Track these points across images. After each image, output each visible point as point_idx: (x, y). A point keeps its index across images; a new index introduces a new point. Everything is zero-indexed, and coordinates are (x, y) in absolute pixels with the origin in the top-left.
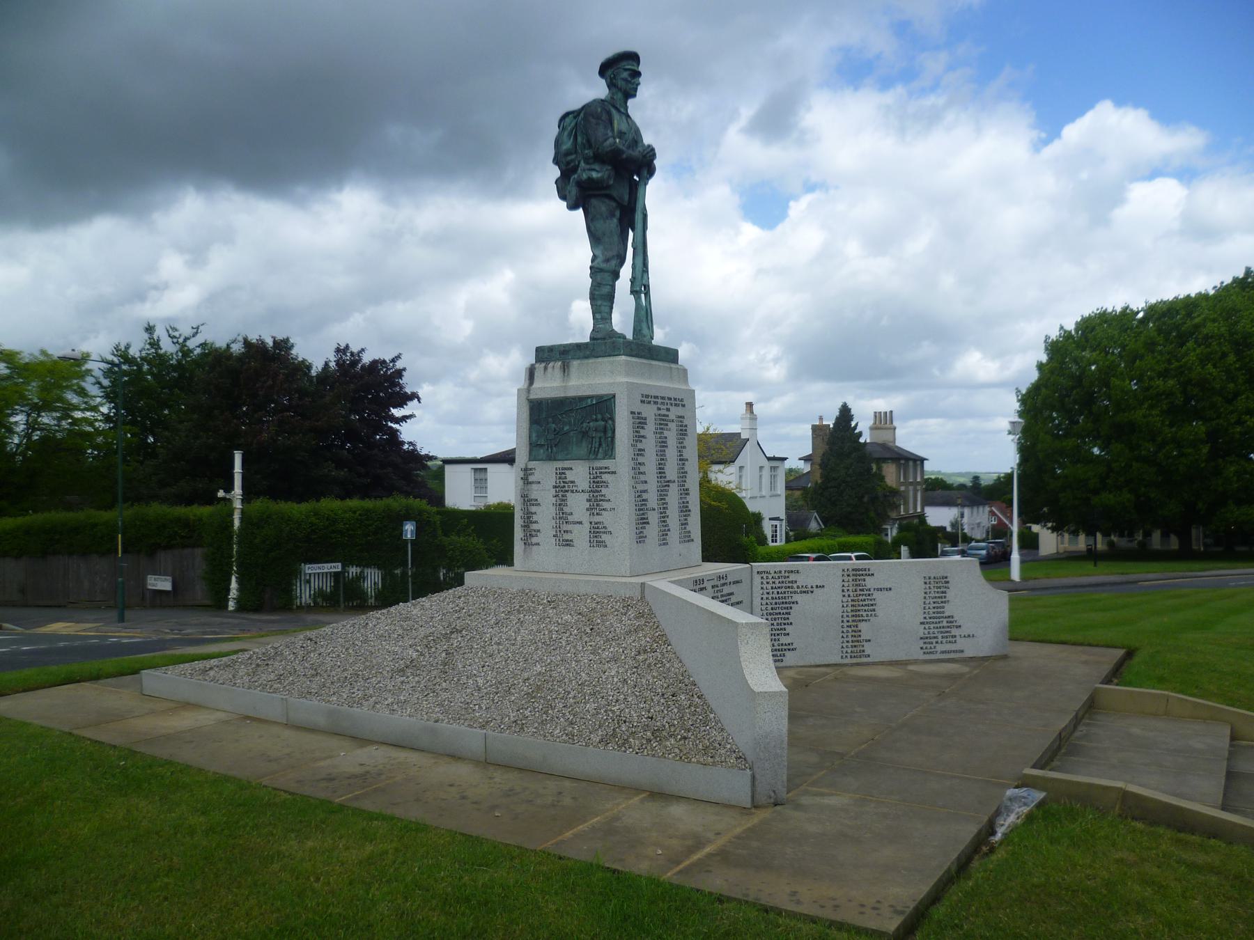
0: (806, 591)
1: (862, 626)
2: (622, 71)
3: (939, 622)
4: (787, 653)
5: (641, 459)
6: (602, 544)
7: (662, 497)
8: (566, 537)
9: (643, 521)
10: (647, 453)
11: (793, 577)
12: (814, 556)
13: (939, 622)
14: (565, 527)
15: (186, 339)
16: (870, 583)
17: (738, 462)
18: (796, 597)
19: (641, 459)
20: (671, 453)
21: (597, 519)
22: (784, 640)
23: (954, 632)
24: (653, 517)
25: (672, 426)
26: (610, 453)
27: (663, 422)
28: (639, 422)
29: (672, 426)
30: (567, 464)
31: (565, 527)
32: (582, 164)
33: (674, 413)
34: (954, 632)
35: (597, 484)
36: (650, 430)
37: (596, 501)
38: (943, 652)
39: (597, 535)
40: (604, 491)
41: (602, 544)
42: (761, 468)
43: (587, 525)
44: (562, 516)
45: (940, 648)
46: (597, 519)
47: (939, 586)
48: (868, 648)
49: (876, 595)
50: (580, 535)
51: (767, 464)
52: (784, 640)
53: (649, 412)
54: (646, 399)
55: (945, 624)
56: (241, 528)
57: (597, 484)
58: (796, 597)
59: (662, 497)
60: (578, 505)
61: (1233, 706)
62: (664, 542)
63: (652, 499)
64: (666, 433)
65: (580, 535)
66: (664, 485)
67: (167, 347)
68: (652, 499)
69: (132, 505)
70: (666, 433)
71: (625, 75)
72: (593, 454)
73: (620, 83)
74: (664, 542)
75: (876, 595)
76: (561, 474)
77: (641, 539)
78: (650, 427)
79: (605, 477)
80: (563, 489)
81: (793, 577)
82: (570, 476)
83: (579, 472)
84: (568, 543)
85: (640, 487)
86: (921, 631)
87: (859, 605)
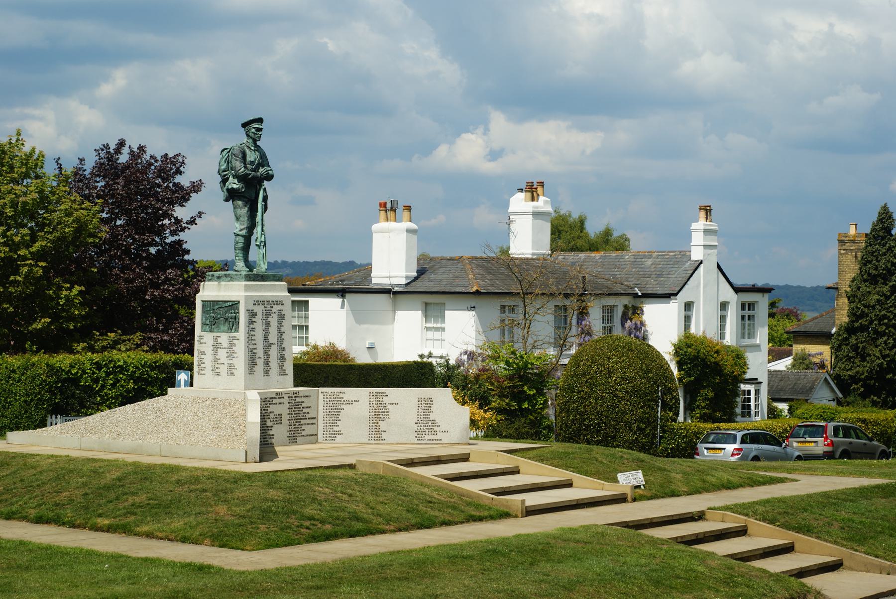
0: (348, 403)
1: (380, 423)
2: (253, 126)
3: (426, 424)
5: (252, 333)
6: (232, 374)
7: (266, 352)
8: (218, 370)
9: (253, 363)
10: (257, 330)
11: (341, 395)
13: (426, 424)
14: (217, 366)
16: (386, 400)
17: (684, 296)
18: (343, 406)
19: (252, 333)
20: (273, 330)
21: (231, 362)
22: (336, 429)
23: (436, 429)
24: (260, 362)
25: (274, 315)
26: (237, 330)
27: (268, 314)
28: (252, 314)
29: (274, 315)
30: (218, 334)
31: (217, 366)
32: (231, 178)
33: (275, 308)
34: (436, 429)
35: (232, 344)
36: (259, 319)
37: (231, 354)
39: (231, 368)
40: (234, 348)
41: (232, 374)
42: (724, 306)
43: (226, 365)
44: (216, 360)
45: (427, 437)
46: (231, 362)
47: (428, 403)
48: (384, 435)
49: (389, 407)
50: (223, 369)
51: (728, 294)
52: (336, 429)
53: (259, 310)
54: (257, 303)
57: (232, 344)
58: (343, 406)
59: (266, 352)
60: (222, 354)
62: (267, 372)
63: (260, 352)
64: (269, 319)
65: (223, 369)
66: (268, 345)
68: (260, 352)
70: (269, 319)
71: (253, 130)
72: (230, 330)
73: (251, 134)
74: (267, 372)
75: (389, 407)
76: (216, 338)
77: (251, 372)
78: (259, 319)
79: (235, 341)
80: (216, 346)
81: (341, 395)
82: (219, 340)
83: (224, 338)
84: (218, 374)
85: (252, 347)
86: (416, 427)
87: (379, 414)
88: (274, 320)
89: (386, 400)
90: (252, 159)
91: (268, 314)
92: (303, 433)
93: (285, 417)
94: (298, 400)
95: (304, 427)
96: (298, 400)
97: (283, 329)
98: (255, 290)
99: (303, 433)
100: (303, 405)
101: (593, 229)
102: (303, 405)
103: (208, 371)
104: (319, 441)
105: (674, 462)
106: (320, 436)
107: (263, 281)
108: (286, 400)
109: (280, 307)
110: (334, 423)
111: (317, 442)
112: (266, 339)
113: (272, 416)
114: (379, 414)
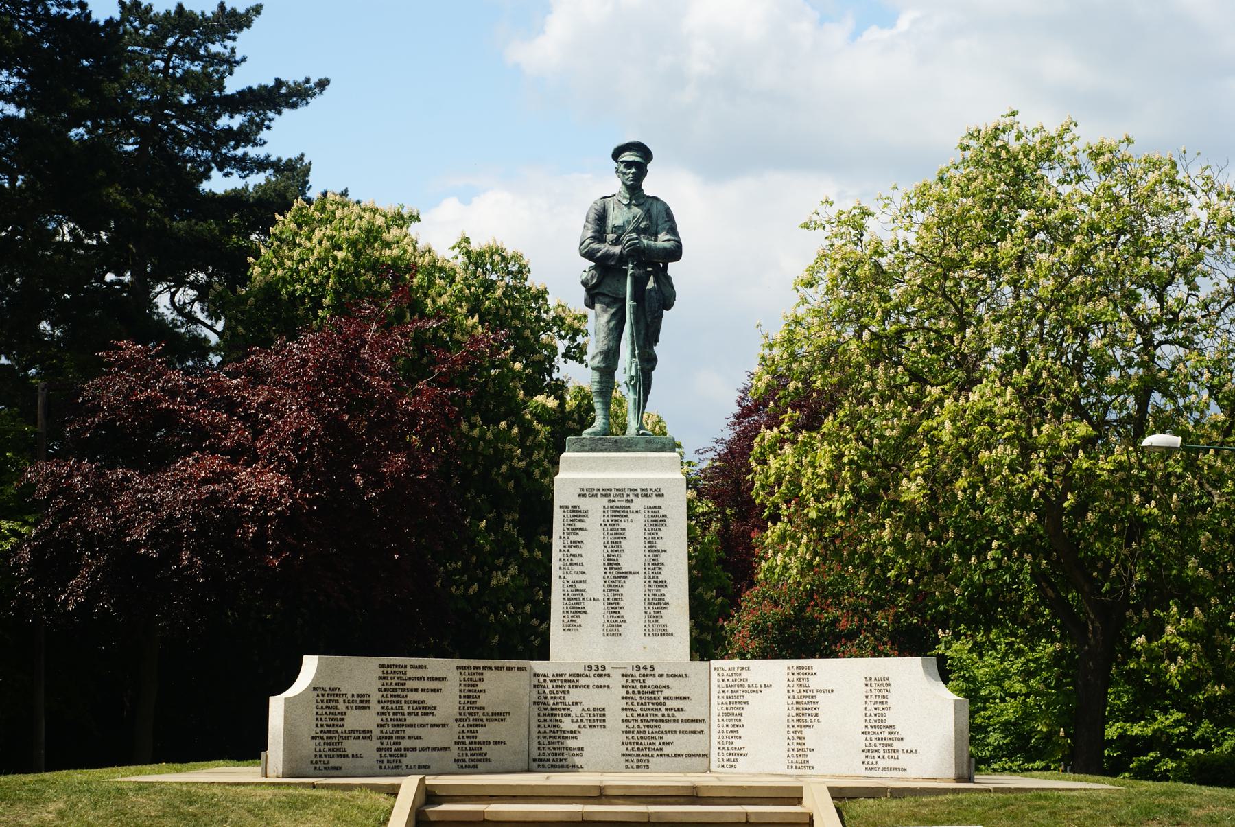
1: (806, 732)
2: (635, 159)
3: (881, 735)
4: (739, 758)
11: (744, 674)
12: (1076, 793)
13: (881, 735)
15: (1089, 178)
16: (813, 683)
18: (748, 697)
22: (737, 743)
27: (617, 515)
33: (639, 503)
38: (884, 769)
45: (882, 763)
47: (880, 689)
52: (737, 743)
55: (886, 735)
56: (126, 152)
58: (748, 697)
61: (1041, 794)
66: (616, 576)
67: (720, 448)
69: (268, 157)
75: (820, 697)
81: (744, 674)
87: (804, 712)
88: (635, 529)
89: (813, 683)
90: (619, 222)
91: (617, 515)
92: (667, 750)
93: (615, 717)
94: (650, 681)
95: (667, 738)
96: (650, 681)
97: (660, 545)
98: (591, 469)
99: (667, 750)
100: (666, 693)
101: (405, 213)
102: (666, 693)
103: (596, 612)
104: (713, 768)
105: (69, 790)
106: (714, 757)
107: (619, 450)
108: (616, 681)
109: (654, 501)
110: (733, 734)
111: (708, 769)
112: (612, 562)
113: (576, 710)
114: (804, 712)
